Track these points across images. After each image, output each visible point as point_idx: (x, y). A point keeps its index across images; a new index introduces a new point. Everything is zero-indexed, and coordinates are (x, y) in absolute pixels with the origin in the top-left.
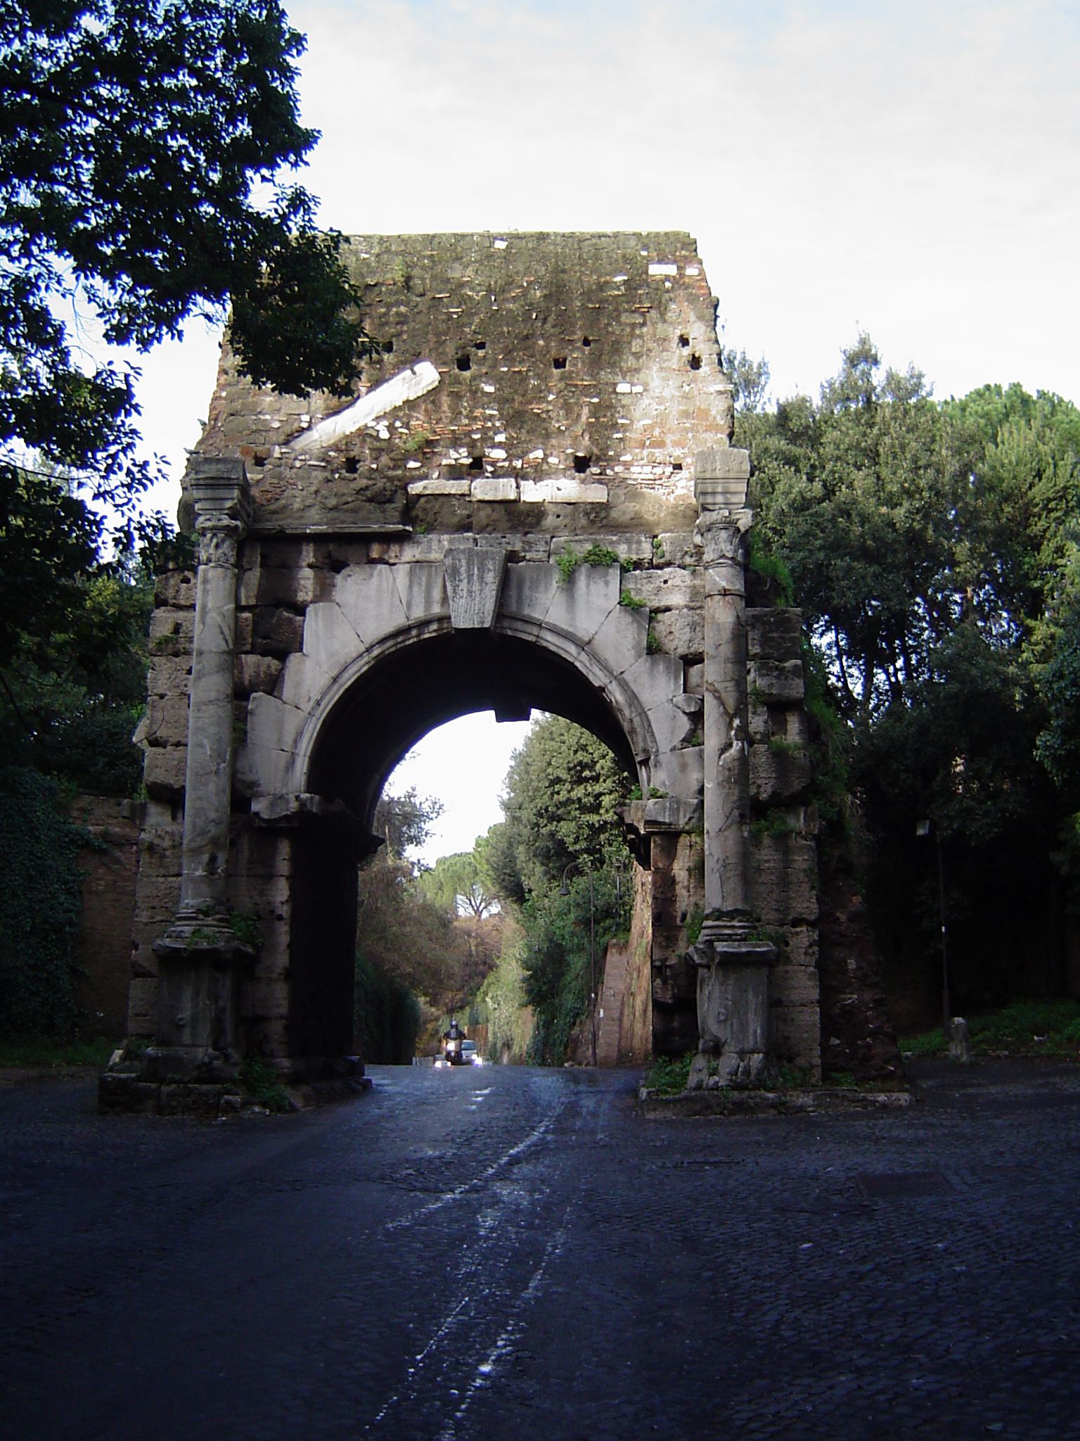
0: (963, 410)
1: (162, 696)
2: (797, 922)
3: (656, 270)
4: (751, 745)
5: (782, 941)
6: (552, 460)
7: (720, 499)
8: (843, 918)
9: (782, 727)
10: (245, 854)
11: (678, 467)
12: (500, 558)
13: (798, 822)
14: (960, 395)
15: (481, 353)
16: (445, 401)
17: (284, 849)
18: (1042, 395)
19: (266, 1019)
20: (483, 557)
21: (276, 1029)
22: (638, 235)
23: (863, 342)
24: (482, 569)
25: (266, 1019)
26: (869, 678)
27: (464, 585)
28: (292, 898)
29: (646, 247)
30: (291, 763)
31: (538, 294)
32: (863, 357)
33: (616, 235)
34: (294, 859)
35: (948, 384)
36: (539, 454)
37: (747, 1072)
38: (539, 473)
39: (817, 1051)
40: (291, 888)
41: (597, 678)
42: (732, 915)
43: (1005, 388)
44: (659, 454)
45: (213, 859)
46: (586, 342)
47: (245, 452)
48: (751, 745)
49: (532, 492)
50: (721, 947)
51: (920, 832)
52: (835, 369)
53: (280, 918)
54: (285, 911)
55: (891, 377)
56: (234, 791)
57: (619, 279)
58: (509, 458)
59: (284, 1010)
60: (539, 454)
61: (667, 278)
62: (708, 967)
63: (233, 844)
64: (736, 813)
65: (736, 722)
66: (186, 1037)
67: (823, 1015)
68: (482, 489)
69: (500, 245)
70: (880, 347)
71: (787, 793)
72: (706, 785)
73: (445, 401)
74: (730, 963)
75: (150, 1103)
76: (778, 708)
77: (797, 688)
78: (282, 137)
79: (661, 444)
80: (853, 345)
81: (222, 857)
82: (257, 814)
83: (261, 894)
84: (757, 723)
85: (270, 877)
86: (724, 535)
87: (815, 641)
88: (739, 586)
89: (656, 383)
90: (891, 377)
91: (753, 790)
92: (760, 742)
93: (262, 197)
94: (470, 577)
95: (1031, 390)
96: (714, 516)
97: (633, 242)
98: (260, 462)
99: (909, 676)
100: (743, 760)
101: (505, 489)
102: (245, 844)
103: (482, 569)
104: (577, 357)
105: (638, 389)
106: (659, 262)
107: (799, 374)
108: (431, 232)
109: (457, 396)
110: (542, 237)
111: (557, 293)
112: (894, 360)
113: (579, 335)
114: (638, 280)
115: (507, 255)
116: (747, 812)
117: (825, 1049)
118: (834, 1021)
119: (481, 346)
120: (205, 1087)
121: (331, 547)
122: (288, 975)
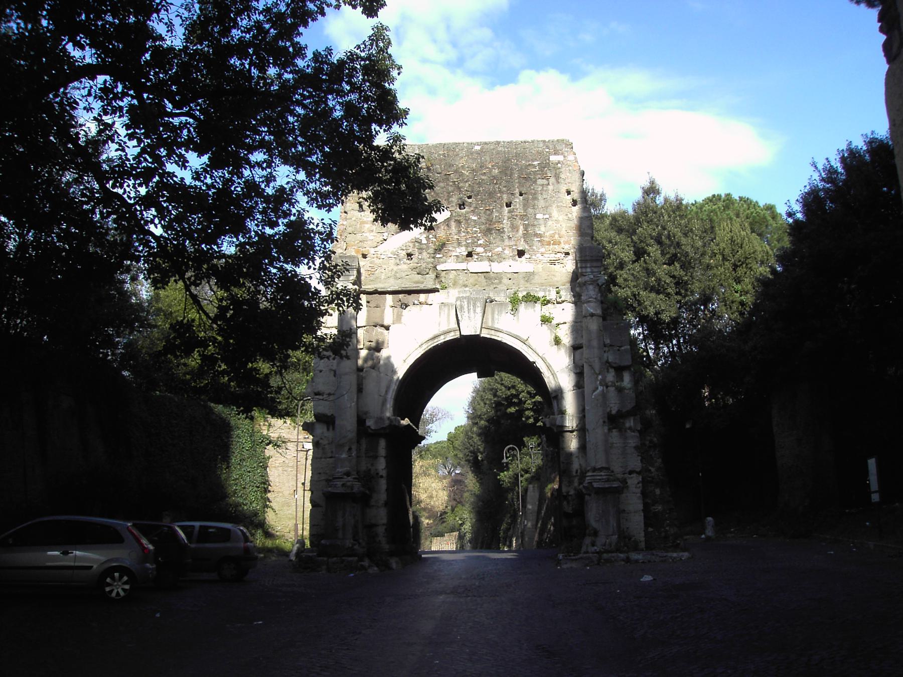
0: (701, 208)
1: (321, 371)
2: (631, 473)
3: (553, 158)
4: (607, 387)
5: (624, 481)
6: (507, 252)
7: (589, 270)
8: (653, 470)
9: (621, 379)
10: (364, 446)
11: (567, 254)
12: (483, 301)
13: (630, 423)
14: (700, 200)
15: (470, 200)
16: (453, 224)
17: (382, 443)
18: (741, 198)
19: (376, 525)
20: (476, 300)
21: (381, 530)
22: (544, 141)
23: (652, 183)
24: (475, 306)
25: (376, 525)
26: (657, 349)
27: (466, 314)
28: (387, 467)
29: (548, 147)
30: (384, 403)
31: (497, 171)
32: (651, 190)
33: (533, 142)
34: (388, 447)
35: (694, 192)
36: (500, 249)
37: (610, 544)
38: (500, 258)
39: (643, 534)
40: (387, 463)
41: (531, 357)
42: (601, 469)
43: (723, 196)
44: (557, 248)
45: (350, 449)
46: (521, 194)
47: (357, 252)
48: (607, 387)
49: (496, 267)
50: (595, 485)
51: (688, 426)
52: (638, 195)
53: (382, 477)
54: (383, 473)
55: (666, 200)
56: (358, 416)
57: (536, 163)
58: (485, 251)
59: (385, 521)
60: (500, 249)
61: (559, 162)
62: (590, 495)
63: (358, 442)
64: (601, 421)
65: (600, 377)
66: (340, 535)
67: (645, 517)
68: (474, 266)
69: (478, 148)
70: (661, 184)
71: (624, 411)
72: (587, 408)
73: (453, 224)
74: (600, 492)
75: (324, 567)
76: (619, 370)
77: (627, 361)
78: (389, 111)
79: (559, 243)
80: (647, 184)
81: (354, 447)
82: (369, 427)
83: (372, 465)
84: (611, 377)
85: (376, 457)
86: (591, 287)
87: (632, 332)
88: (599, 312)
89: (555, 213)
90: (666, 200)
91: (608, 410)
92: (612, 386)
93: (381, 140)
94: (469, 310)
95: (736, 196)
96: (587, 278)
97: (541, 145)
98: (364, 256)
99: (679, 348)
100: (604, 395)
101: (483, 266)
102: (364, 442)
103: (475, 306)
104: (518, 201)
105: (547, 216)
106: (555, 154)
107: (620, 199)
108: (443, 142)
109: (459, 222)
110: (498, 143)
111: (506, 170)
112: (668, 191)
113: (517, 191)
114: (545, 165)
115: (480, 153)
116: (606, 420)
117: (646, 531)
118: (650, 519)
119: (470, 197)
120: (350, 559)
121: (401, 296)
122: (386, 504)
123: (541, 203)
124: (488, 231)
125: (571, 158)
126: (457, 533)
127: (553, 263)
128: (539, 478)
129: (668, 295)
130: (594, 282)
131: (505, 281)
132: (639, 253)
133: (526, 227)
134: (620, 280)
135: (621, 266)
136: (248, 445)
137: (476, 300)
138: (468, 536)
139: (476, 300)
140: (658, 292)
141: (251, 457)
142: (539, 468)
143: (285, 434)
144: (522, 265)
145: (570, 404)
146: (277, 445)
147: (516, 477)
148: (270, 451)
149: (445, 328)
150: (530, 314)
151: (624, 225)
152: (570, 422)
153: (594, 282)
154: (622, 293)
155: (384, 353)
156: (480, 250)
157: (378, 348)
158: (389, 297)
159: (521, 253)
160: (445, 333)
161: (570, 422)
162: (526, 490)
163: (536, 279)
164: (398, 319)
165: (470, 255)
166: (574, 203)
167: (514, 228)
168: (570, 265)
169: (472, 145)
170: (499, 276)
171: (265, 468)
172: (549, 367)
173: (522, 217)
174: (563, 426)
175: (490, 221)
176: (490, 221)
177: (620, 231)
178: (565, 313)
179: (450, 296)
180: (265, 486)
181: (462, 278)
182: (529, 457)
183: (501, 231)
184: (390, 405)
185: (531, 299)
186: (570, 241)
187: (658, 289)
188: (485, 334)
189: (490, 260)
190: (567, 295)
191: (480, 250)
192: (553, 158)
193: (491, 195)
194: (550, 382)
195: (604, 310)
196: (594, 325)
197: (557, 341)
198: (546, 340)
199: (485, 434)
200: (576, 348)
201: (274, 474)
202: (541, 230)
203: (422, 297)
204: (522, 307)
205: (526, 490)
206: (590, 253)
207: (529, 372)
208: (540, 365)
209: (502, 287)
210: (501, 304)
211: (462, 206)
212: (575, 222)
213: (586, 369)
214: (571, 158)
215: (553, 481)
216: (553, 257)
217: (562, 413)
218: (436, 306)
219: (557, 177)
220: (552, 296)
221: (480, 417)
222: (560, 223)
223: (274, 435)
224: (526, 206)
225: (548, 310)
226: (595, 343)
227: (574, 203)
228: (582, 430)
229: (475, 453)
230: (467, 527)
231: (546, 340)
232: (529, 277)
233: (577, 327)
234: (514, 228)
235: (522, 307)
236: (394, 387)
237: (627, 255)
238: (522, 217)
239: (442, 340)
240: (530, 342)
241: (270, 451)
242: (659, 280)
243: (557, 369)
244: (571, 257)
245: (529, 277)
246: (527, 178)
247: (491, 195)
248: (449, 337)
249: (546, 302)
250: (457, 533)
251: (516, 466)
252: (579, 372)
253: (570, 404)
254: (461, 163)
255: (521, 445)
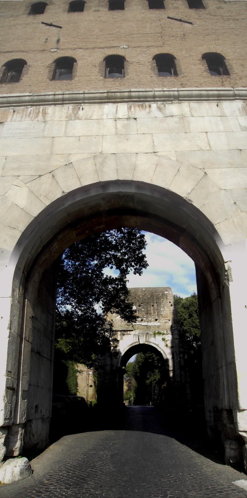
3: (166, 292)
30: (118, 362)
38: (151, 321)
41: (159, 350)
49: (149, 324)
68: (143, 323)
100: (180, 361)
101: (146, 324)
104: (155, 305)
111: (152, 296)
114: (163, 294)
123: (162, 306)
124: (147, 314)
125: (171, 292)
126: (128, 401)
127: (165, 323)
128: (160, 382)
129: (199, 329)
130: (177, 329)
131: (152, 328)
132: (191, 316)
133: (158, 312)
134: (184, 324)
135: (185, 319)
136: (72, 373)
137: (144, 334)
138: (132, 402)
139: (144, 334)
140: (196, 328)
141: (73, 376)
142: (159, 379)
143: (82, 369)
144: (157, 323)
145: (171, 363)
146: (80, 372)
147: (151, 382)
148: (78, 374)
149: (135, 341)
150: (159, 338)
151: (185, 306)
152: (171, 368)
153: (177, 329)
154: (185, 328)
155: (118, 348)
156: (145, 319)
157: (116, 347)
158: (119, 332)
159: (156, 320)
160: (135, 343)
161: (171, 368)
162: (155, 386)
163: (161, 327)
164: (122, 339)
165: (142, 320)
166: (172, 305)
167: (154, 313)
168: (170, 323)
169: (142, 288)
170: (150, 326)
171: (77, 379)
172: (164, 353)
173: (157, 310)
174: (169, 370)
175: (148, 311)
176: (148, 311)
177: (185, 308)
178: (169, 337)
179: (137, 332)
180: (76, 385)
181: (140, 327)
182: (156, 376)
183: (151, 314)
184: (119, 363)
185: (159, 333)
186: (171, 317)
187: (196, 327)
188: (146, 343)
189: (148, 322)
190: (169, 332)
191: (145, 319)
192: (166, 292)
193: (148, 303)
194: (165, 357)
195: (180, 337)
196: (177, 341)
197: (167, 346)
198: (163, 345)
199: (140, 367)
200: (172, 347)
201: (79, 381)
202: (162, 313)
203: (129, 332)
204: (157, 336)
205: (155, 386)
206: (175, 313)
207: (159, 354)
208: (162, 352)
209: (151, 330)
210: (151, 335)
211: (140, 306)
212: (172, 311)
213: (175, 354)
214: (171, 292)
215: (164, 384)
216: (165, 321)
217: (168, 366)
218: (132, 335)
219: (167, 298)
220: (165, 332)
221: (139, 362)
222: (168, 311)
223: (79, 369)
224: (158, 306)
225: (164, 336)
226: (177, 346)
227: (172, 305)
228: (174, 371)
229: (136, 373)
230: (132, 398)
231: (163, 345)
232: (158, 327)
233: (173, 342)
234: (154, 313)
235: (157, 336)
236: (121, 358)
237: (187, 316)
238: (157, 310)
239: (134, 345)
240: (159, 345)
241: (78, 374)
242: (196, 325)
243: (167, 353)
244: (171, 321)
245: (158, 327)
246: (158, 298)
247: (148, 303)
248: (136, 344)
249: (163, 334)
250: (128, 401)
251: (152, 378)
252: (173, 354)
253: (171, 363)
254: (139, 293)
255: (154, 372)
